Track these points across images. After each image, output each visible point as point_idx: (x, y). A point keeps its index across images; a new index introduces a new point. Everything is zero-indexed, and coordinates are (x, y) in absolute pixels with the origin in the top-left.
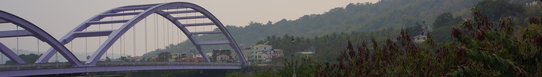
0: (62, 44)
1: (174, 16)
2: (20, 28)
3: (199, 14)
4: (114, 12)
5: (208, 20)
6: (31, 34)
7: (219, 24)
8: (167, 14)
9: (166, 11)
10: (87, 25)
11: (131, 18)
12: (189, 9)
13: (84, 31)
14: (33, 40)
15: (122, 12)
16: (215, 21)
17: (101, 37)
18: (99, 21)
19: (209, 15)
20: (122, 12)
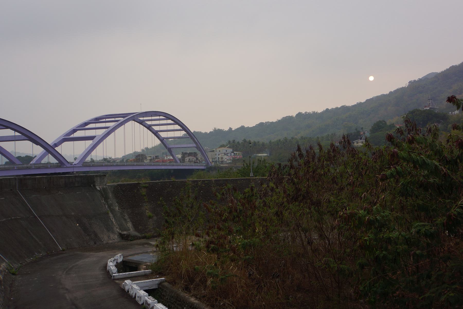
2: (17, 134)
4: (97, 120)
6: (27, 138)
9: (141, 119)
10: (74, 131)
11: (112, 125)
12: (161, 117)
15: (104, 120)
16: (184, 128)
18: (84, 128)
19: (179, 122)
20: (104, 120)
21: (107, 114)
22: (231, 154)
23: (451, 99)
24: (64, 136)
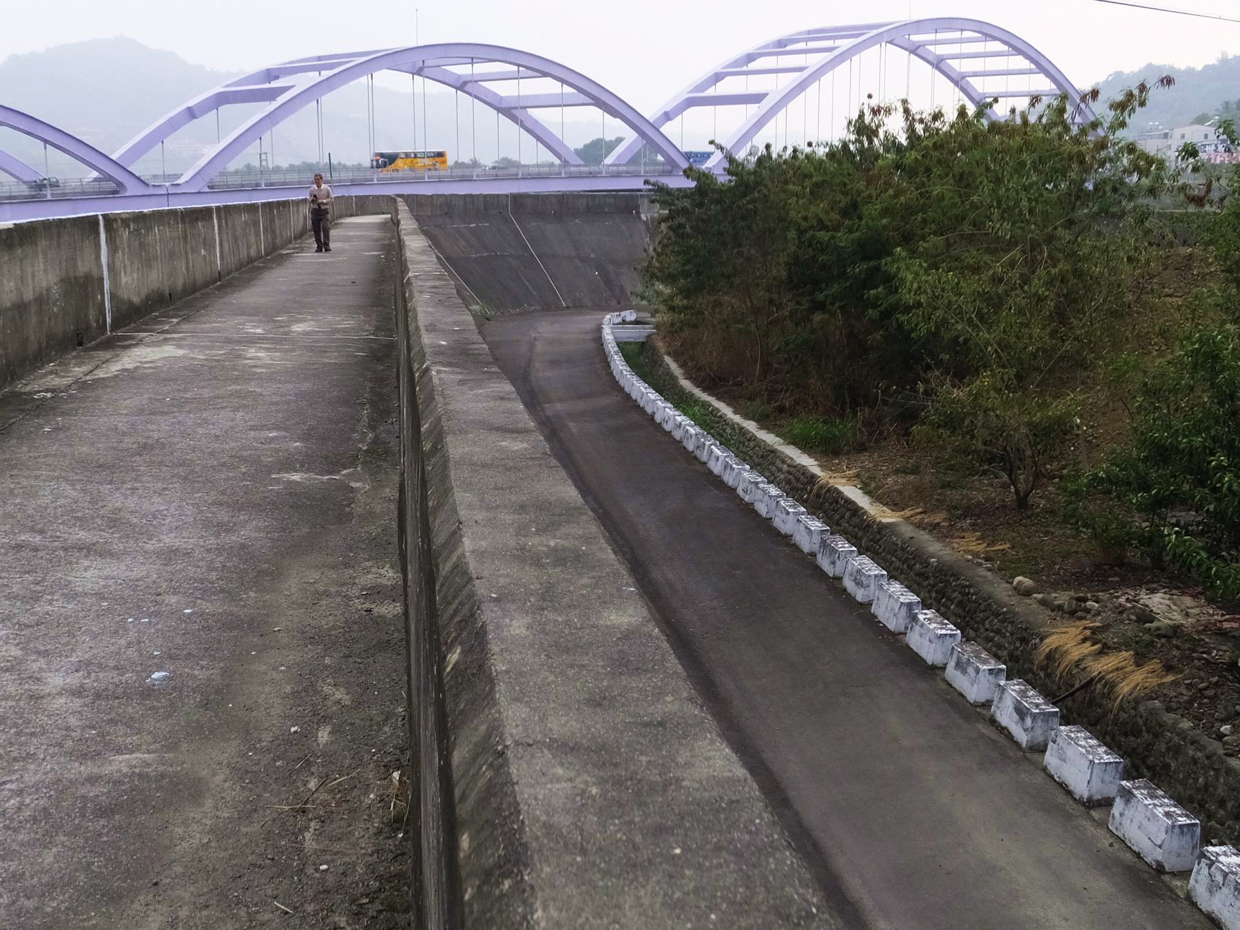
0: (120, 166)
1: (940, 50)
2: (568, 90)
3: (997, 46)
4: (781, 46)
5: (1020, 62)
6: (592, 101)
7: (1053, 71)
8: (919, 47)
9: (914, 38)
10: (718, 77)
11: (815, 60)
12: (967, 34)
13: (711, 92)
14: (595, 112)
15: (801, 46)
16: (1042, 65)
17: (718, 107)
18: (745, 68)
19: (1024, 48)
20: (801, 46)
21: (811, 27)
22: (1216, 146)
23: (712, 142)
24: (691, 92)
